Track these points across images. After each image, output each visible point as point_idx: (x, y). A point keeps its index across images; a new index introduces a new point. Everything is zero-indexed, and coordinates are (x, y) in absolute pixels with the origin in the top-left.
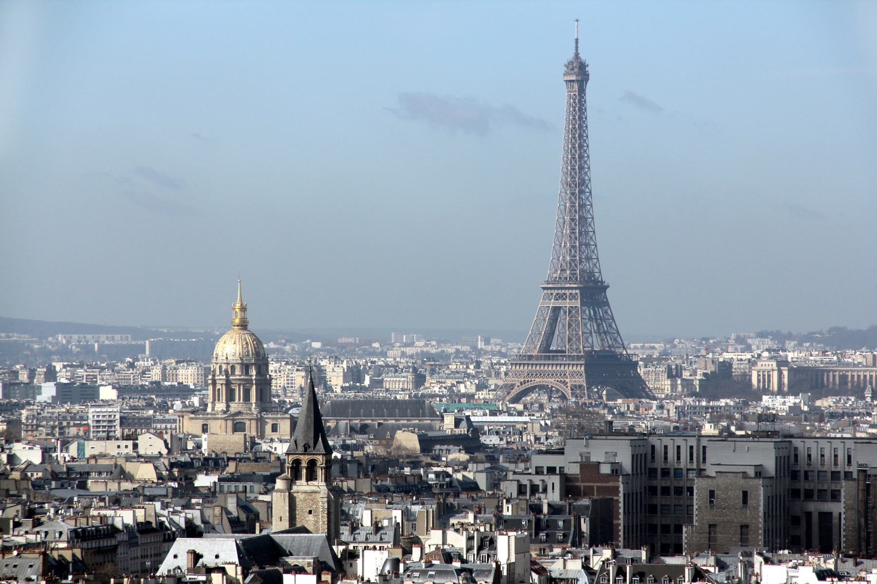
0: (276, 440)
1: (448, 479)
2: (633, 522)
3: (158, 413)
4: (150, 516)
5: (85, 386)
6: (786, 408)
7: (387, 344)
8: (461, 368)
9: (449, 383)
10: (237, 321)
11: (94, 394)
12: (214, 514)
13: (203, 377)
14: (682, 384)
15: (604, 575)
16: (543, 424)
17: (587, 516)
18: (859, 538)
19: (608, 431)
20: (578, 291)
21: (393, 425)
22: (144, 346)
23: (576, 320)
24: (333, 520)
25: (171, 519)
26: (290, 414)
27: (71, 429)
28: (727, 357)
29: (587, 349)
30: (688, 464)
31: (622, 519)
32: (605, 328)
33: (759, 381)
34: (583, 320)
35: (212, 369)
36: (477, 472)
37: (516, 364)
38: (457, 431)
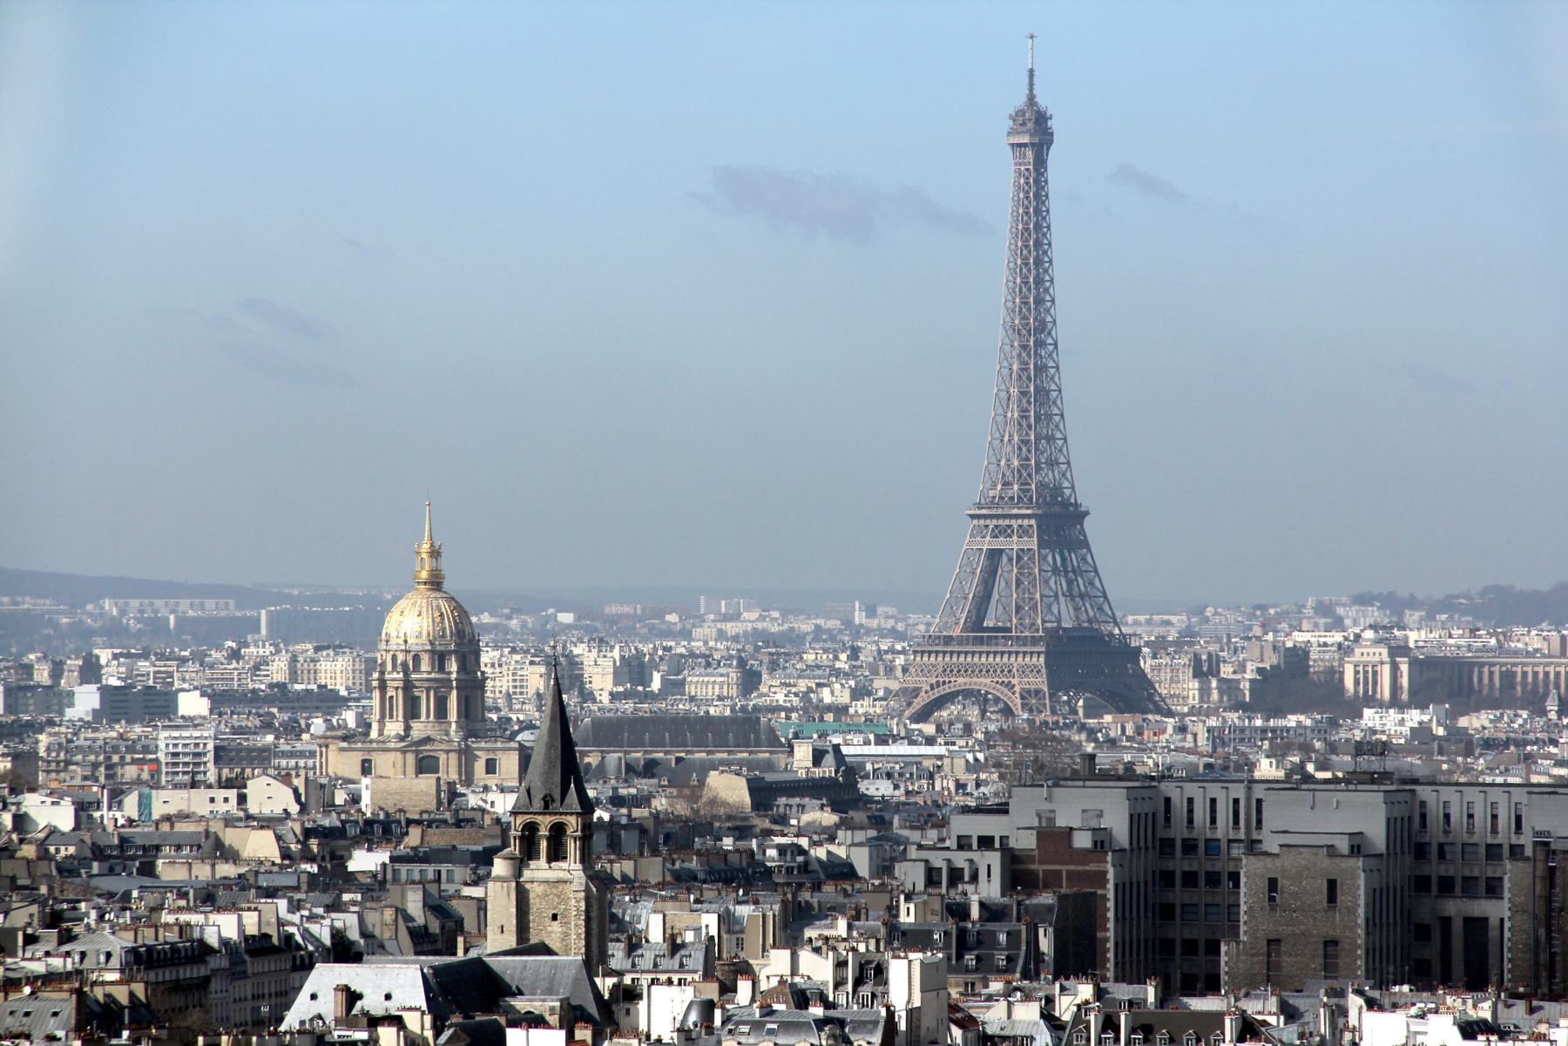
0: (494, 788)
1: (800, 859)
2: (1131, 934)
3: (282, 741)
4: (268, 924)
5: (152, 691)
6: (1406, 730)
7: (692, 616)
8: (825, 658)
9: (802, 685)
10: (424, 575)
11: (168, 707)
12: (382, 920)
13: (363, 675)
14: (1219, 688)
15: (1080, 1031)
16: (971, 760)
17: (1050, 925)
18: (1537, 963)
19: (1087, 773)
20: (1033, 522)
21: (702, 761)
22: (258, 620)
23: (1030, 574)
24: (595, 931)
25: (306, 930)
26: (519, 742)
27: (127, 768)
28: (1300, 639)
29: (1049, 625)
30: (1231, 830)
31: (1112, 930)
32: (1082, 588)
33: (1357, 682)
34: (1043, 574)
35: (379, 661)
36: (853, 845)
37: (923, 653)
38: (818, 773)
